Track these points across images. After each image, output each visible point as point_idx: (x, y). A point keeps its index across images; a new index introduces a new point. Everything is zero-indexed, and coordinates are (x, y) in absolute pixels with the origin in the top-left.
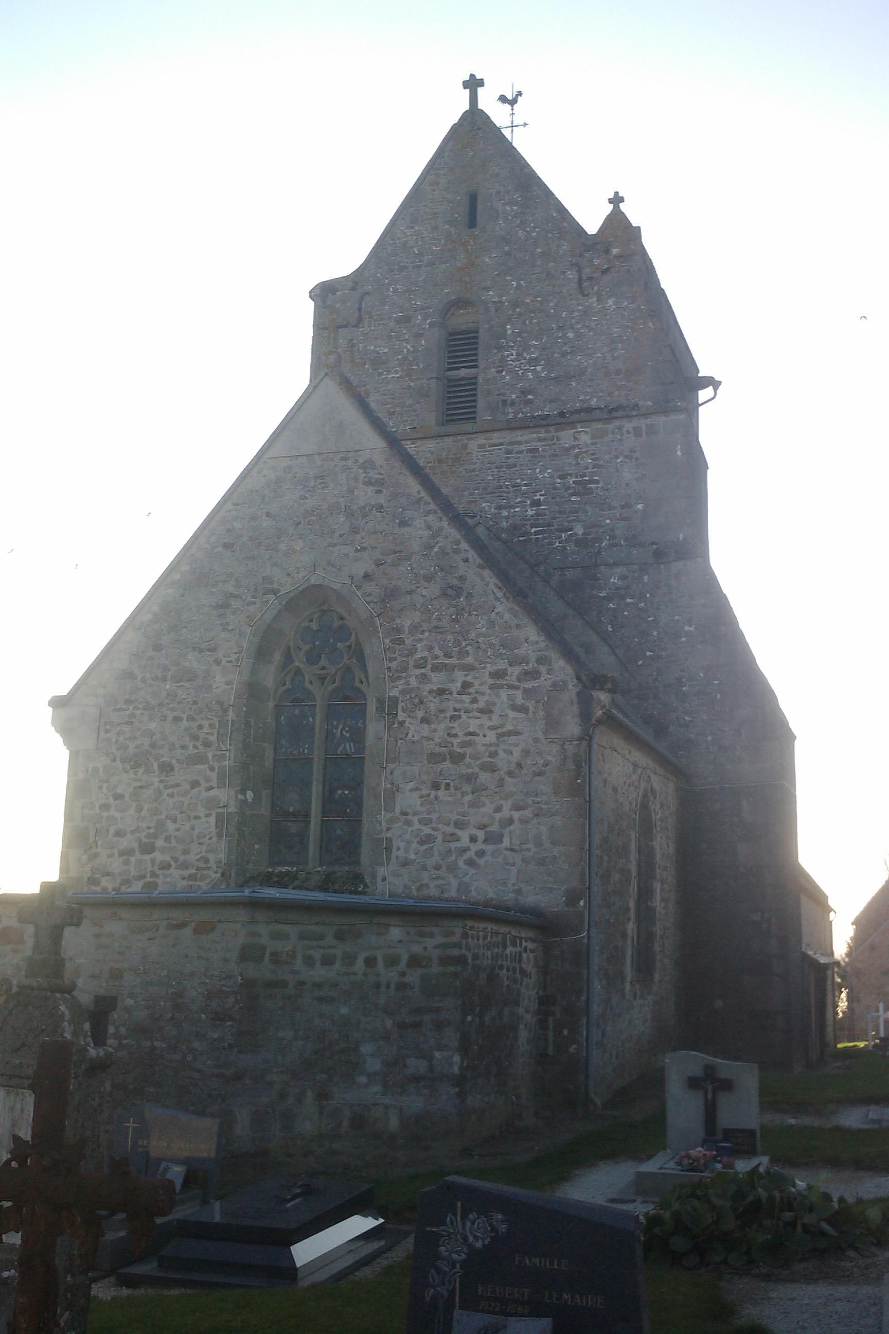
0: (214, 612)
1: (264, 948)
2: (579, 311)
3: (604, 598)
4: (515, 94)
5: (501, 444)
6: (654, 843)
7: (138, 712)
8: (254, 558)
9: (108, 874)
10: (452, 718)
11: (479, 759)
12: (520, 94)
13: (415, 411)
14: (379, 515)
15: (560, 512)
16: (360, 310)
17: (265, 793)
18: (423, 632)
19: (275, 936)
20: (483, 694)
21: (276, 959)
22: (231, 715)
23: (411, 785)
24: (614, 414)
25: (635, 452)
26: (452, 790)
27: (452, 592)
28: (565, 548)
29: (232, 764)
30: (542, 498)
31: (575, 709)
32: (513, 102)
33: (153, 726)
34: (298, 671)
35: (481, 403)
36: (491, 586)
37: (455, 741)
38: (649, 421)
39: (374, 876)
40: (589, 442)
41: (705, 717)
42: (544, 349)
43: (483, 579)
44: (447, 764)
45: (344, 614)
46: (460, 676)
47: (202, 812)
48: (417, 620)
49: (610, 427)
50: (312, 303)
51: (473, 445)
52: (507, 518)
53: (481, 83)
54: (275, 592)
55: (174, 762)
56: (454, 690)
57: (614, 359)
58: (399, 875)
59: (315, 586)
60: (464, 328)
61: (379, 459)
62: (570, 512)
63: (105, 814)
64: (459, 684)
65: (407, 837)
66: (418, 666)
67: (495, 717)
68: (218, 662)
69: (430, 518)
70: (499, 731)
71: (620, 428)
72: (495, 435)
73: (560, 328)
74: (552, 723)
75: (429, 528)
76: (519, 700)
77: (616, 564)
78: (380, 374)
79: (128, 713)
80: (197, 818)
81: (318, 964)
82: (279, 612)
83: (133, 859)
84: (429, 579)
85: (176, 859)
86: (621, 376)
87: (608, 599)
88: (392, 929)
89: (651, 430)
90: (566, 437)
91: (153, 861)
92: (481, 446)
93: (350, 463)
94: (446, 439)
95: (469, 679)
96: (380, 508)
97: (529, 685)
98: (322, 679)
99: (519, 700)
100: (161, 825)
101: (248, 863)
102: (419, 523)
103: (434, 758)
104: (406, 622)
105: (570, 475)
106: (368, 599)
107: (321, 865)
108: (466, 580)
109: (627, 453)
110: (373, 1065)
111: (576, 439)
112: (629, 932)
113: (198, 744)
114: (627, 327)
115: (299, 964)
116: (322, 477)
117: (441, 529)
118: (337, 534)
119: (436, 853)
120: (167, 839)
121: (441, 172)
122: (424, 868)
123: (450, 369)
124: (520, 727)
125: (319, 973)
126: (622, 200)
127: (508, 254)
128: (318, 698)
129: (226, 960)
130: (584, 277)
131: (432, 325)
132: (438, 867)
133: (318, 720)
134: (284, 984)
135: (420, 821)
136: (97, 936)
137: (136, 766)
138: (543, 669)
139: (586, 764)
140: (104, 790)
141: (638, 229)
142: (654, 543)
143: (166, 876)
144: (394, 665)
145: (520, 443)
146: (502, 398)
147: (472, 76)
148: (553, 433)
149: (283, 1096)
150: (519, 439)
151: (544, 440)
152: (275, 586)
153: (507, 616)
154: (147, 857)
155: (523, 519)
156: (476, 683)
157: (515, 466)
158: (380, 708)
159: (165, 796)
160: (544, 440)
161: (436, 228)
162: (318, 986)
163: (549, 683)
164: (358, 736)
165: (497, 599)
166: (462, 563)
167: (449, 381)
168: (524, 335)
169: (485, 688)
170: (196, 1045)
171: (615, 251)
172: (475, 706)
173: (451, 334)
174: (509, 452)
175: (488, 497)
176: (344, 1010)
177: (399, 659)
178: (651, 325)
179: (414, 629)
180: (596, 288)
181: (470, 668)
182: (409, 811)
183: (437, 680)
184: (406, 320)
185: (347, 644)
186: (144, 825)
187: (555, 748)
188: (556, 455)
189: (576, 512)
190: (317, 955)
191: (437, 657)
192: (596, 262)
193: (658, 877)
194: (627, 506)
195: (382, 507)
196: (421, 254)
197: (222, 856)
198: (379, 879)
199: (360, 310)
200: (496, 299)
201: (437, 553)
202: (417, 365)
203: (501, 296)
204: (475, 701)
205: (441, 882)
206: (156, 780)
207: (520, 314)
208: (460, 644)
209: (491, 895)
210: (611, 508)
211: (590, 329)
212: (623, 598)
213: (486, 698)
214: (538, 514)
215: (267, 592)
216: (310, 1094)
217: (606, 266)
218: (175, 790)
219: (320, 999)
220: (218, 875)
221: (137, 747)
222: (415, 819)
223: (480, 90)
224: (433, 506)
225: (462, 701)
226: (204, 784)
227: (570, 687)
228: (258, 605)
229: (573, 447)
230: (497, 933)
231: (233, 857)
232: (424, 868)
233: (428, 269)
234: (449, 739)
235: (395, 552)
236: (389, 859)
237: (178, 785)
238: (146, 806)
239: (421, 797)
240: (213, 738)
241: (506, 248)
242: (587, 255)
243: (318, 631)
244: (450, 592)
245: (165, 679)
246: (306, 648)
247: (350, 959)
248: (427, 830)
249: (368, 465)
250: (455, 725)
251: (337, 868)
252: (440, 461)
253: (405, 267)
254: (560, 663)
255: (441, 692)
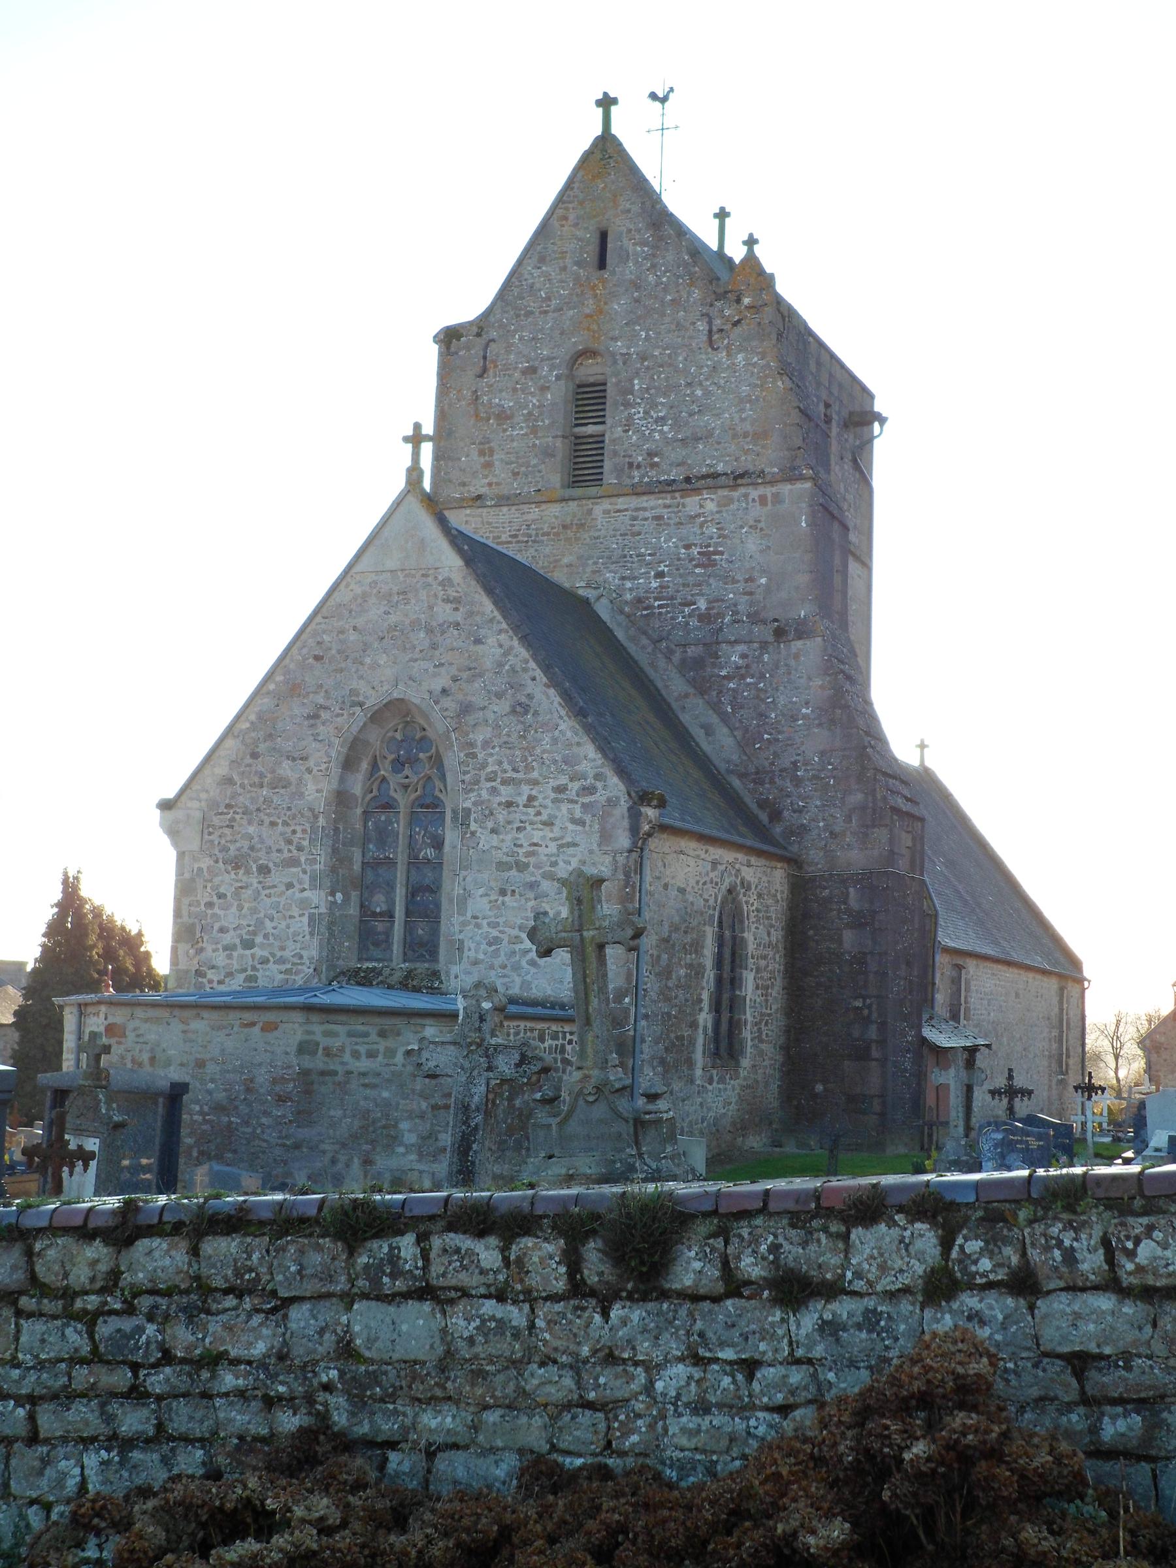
0: (306, 723)
1: (318, 1044)
2: (707, 366)
3: (724, 677)
4: (667, 89)
5: (626, 510)
6: (745, 935)
7: (237, 817)
8: (341, 670)
9: (213, 967)
10: (518, 829)
11: (541, 868)
12: (672, 90)
13: (540, 472)
14: (456, 632)
15: (684, 585)
16: (485, 358)
17: (355, 895)
18: (493, 748)
19: (327, 1034)
20: (545, 807)
21: (328, 1052)
22: (322, 821)
23: (481, 891)
24: (739, 481)
25: (759, 521)
26: (517, 896)
27: (521, 709)
28: (687, 623)
29: (322, 867)
30: (666, 569)
31: (626, 823)
32: (664, 100)
33: (251, 830)
34: (384, 779)
35: (608, 465)
36: (556, 704)
37: (521, 851)
38: (774, 490)
39: (448, 974)
40: (715, 509)
41: (818, 803)
42: (672, 407)
43: (548, 697)
44: (514, 872)
45: (426, 726)
46: (526, 790)
47: (295, 912)
48: (489, 736)
49: (735, 494)
50: (436, 347)
51: (598, 510)
52: (631, 589)
53: (614, 101)
54: (361, 705)
55: (271, 865)
56: (521, 803)
57: (742, 420)
58: (469, 973)
59: (398, 700)
60: (592, 380)
61: (457, 577)
62: (694, 585)
63: (209, 912)
64: (525, 798)
65: (478, 938)
66: (489, 780)
67: (556, 829)
68: (309, 771)
69: (503, 637)
70: (560, 842)
71: (746, 496)
72: (621, 500)
73: (689, 385)
74: (605, 836)
75: (501, 646)
76: (578, 814)
77: (736, 642)
78: (505, 430)
79: (229, 816)
80: (291, 917)
81: (363, 1057)
82: (365, 724)
83: (235, 954)
84: (499, 696)
85: (273, 955)
86: (749, 439)
87: (728, 678)
88: (427, 1028)
89: (778, 500)
90: (691, 503)
91: (253, 956)
92: (606, 512)
93: (430, 579)
94: (571, 503)
95: (534, 793)
96: (457, 625)
97: (586, 800)
98: (406, 787)
99: (578, 814)
100: (259, 923)
101: (338, 959)
102: (491, 641)
103: (502, 866)
104: (479, 737)
105: (695, 545)
106: (445, 714)
107: (405, 961)
108: (532, 698)
109: (752, 523)
110: (411, 1138)
111: (701, 506)
112: (701, 1022)
113: (292, 848)
114: (756, 386)
115: (347, 1057)
116: (404, 593)
117: (511, 648)
118: (417, 650)
119: (502, 953)
120: (266, 936)
121: (570, 206)
122: (492, 967)
123: (577, 425)
124: (577, 839)
125: (364, 1064)
126: (756, 242)
127: (637, 301)
128: (402, 806)
129: (287, 1053)
130: (715, 329)
131: (558, 378)
132: (504, 967)
133: (400, 826)
134: (335, 1073)
135: (489, 924)
136: (184, 1032)
137: (237, 867)
138: (599, 785)
139: (636, 873)
140: (209, 889)
141: (772, 276)
142: (776, 620)
143: (265, 970)
144: (467, 778)
145: (645, 509)
146: (627, 460)
147: (605, 94)
148: (679, 499)
149: (334, 1161)
150: (645, 505)
151: (669, 507)
152: (361, 699)
153: (569, 734)
154: (248, 952)
155: (646, 592)
156: (540, 797)
157: (639, 534)
158: (455, 818)
159: (263, 897)
160: (669, 507)
161: (564, 269)
162: (364, 1074)
163: (604, 798)
164: (438, 844)
165: (561, 717)
166: (529, 682)
167: (577, 438)
168: (652, 391)
169: (548, 802)
170: (264, 1120)
171: (746, 301)
172: (539, 818)
173: (579, 386)
174: (634, 519)
175: (613, 567)
176: (385, 1094)
177: (473, 772)
178: (780, 383)
179: (486, 744)
180: (726, 342)
181: (535, 783)
182: (480, 915)
183: (506, 792)
184: (532, 370)
185: (428, 754)
186: (245, 923)
187: (608, 859)
188: (681, 524)
189: (700, 585)
190: (362, 1049)
191: (505, 771)
192: (727, 313)
193: (750, 966)
194: (750, 580)
195: (458, 624)
196: (548, 299)
197: (315, 953)
198: (452, 977)
199: (485, 358)
200: (625, 351)
201: (508, 671)
202: (543, 421)
203: (629, 348)
204: (539, 813)
205: (507, 980)
206: (255, 881)
207: (648, 368)
208: (526, 760)
209: (549, 992)
210: (735, 581)
211: (719, 387)
212: (743, 677)
213: (549, 811)
214: (661, 587)
215: (354, 704)
216: (356, 1160)
217: (737, 318)
218: (272, 891)
219: (365, 1086)
220: (311, 970)
221: (238, 850)
222: (485, 922)
223: (613, 108)
224: (504, 626)
225: (527, 814)
226: (298, 886)
227: (622, 803)
228: (345, 717)
229: (698, 516)
230: (532, 1030)
231: (325, 954)
232: (492, 967)
233: (556, 315)
234: (515, 849)
235: (470, 669)
236: (461, 959)
237: (275, 886)
238: (246, 905)
239: (490, 902)
240: (306, 843)
241: (636, 294)
242: (718, 304)
243: (402, 741)
244: (518, 709)
245: (262, 786)
246: (391, 757)
247: (391, 1053)
248: (495, 933)
249: (447, 583)
250: (521, 835)
251: (418, 965)
252: (565, 527)
253: (532, 313)
254: (614, 780)
255: (509, 804)
